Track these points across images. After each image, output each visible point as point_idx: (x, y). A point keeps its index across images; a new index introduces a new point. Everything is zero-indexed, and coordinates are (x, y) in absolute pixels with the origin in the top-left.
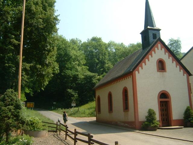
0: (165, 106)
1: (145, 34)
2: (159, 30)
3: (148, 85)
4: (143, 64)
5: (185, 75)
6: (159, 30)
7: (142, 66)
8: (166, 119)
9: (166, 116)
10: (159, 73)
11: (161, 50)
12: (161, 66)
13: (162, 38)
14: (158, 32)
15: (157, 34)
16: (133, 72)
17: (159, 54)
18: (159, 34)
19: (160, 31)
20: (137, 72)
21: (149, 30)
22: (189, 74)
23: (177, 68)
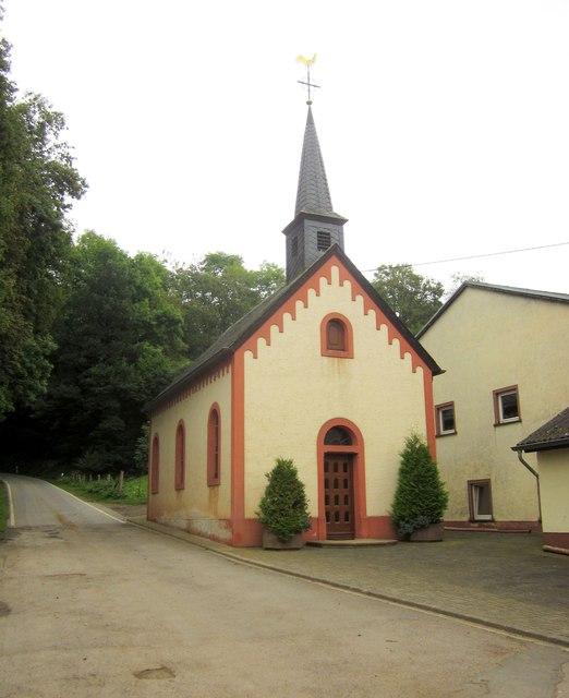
0: (345, 471)
1: (294, 233)
2: (340, 222)
3: (281, 402)
4: (274, 329)
5: (420, 370)
6: (340, 222)
7: (256, 348)
8: (346, 481)
9: (346, 503)
10: (326, 359)
11: (341, 285)
12: (337, 335)
13: (350, 251)
14: (336, 227)
15: (332, 234)
16: (236, 354)
17: (331, 296)
18: (341, 234)
19: (345, 226)
20: (248, 355)
21: (306, 221)
22: (434, 369)
23: (392, 346)
